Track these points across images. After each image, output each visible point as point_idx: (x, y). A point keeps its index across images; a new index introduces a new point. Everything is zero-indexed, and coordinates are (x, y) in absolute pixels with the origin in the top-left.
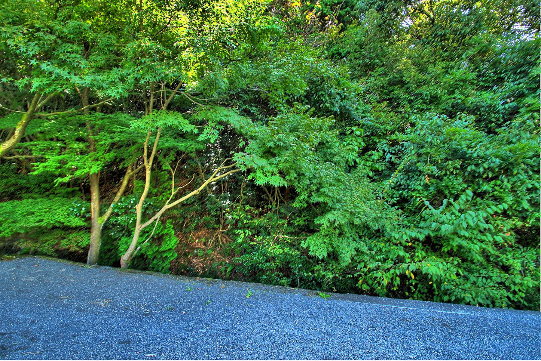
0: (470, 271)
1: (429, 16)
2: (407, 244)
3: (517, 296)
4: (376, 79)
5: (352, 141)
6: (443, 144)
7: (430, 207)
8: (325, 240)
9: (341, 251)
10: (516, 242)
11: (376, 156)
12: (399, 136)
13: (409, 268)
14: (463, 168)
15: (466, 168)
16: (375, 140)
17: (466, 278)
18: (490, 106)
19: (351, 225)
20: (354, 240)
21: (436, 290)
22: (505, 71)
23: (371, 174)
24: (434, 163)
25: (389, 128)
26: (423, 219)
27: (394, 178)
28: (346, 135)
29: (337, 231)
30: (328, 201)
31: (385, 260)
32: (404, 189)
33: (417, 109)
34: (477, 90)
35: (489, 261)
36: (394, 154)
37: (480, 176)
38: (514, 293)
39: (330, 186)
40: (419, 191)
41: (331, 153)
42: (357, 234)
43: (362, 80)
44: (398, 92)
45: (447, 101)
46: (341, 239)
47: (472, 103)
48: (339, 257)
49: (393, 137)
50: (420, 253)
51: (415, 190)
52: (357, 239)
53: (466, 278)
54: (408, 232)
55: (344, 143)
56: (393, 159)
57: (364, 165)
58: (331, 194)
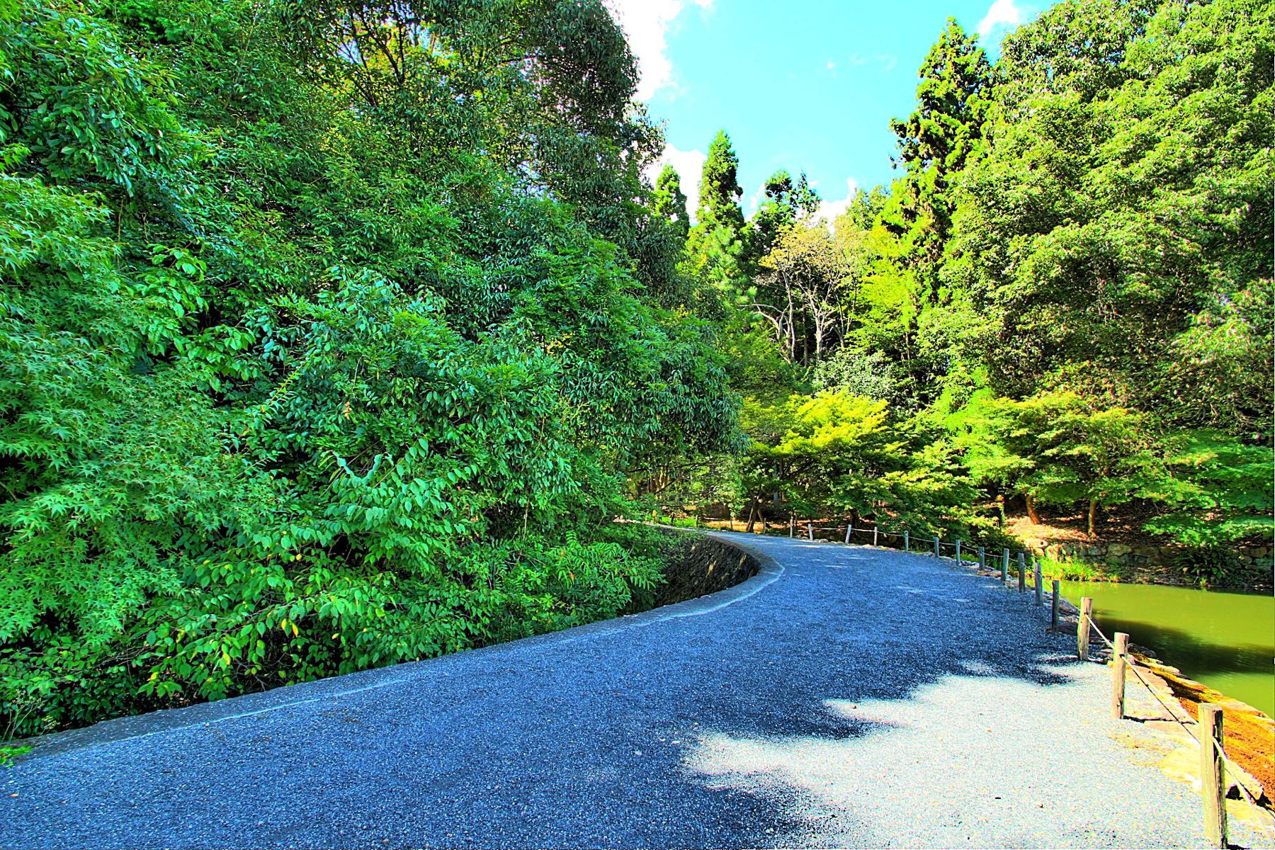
0: (413, 596)
1: (394, 65)
2: (292, 558)
3: (478, 625)
4: (255, 145)
5: (166, 284)
6: (390, 341)
7: (349, 471)
8: (30, 577)
9: (89, 602)
10: (487, 532)
11: (236, 340)
12: (303, 305)
13: (287, 615)
14: (419, 395)
15: (425, 395)
16: (239, 300)
17: (405, 610)
18: (473, 289)
19: (136, 524)
20: (143, 565)
21: (347, 648)
22: (502, 236)
23: (216, 385)
24: (364, 373)
25: (278, 278)
26: (334, 498)
27: (275, 403)
28: (150, 263)
29: (81, 544)
30: (52, 454)
31: (232, 605)
32: (300, 430)
33: (349, 252)
34: (459, 252)
35: (444, 571)
36: (287, 345)
37: (444, 414)
38: (477, 619)
39: (63, 406)
40: (332, 435)
41: (85, 307)
42: (153, 549)
43: (218, 131)
44: (307, 197)
45: (409, 256)
46: (93, 567)
47: (449, 274)
48: (81, 623)
49: (284, 301)
50: (318, 576)
51: (323, 433)
52: (152, 562)
53: (405, 610)
54: (295, 529)
55: (138, 286)
56: (281, 357)
57: (197, 359)
58: (62, 432)
